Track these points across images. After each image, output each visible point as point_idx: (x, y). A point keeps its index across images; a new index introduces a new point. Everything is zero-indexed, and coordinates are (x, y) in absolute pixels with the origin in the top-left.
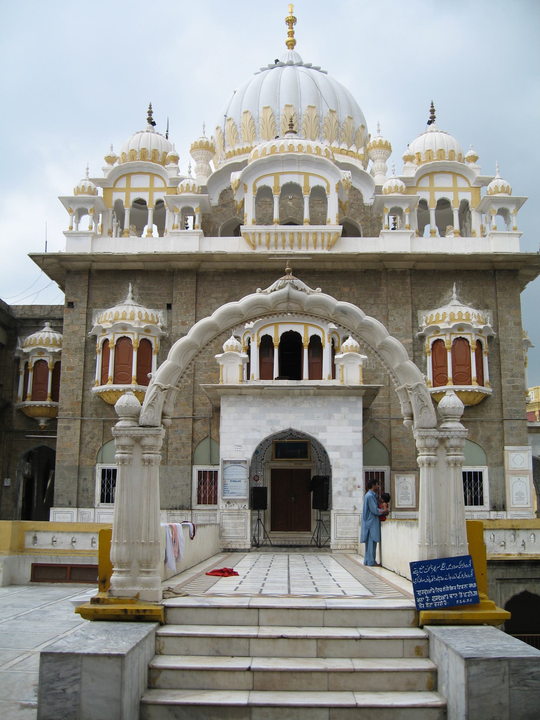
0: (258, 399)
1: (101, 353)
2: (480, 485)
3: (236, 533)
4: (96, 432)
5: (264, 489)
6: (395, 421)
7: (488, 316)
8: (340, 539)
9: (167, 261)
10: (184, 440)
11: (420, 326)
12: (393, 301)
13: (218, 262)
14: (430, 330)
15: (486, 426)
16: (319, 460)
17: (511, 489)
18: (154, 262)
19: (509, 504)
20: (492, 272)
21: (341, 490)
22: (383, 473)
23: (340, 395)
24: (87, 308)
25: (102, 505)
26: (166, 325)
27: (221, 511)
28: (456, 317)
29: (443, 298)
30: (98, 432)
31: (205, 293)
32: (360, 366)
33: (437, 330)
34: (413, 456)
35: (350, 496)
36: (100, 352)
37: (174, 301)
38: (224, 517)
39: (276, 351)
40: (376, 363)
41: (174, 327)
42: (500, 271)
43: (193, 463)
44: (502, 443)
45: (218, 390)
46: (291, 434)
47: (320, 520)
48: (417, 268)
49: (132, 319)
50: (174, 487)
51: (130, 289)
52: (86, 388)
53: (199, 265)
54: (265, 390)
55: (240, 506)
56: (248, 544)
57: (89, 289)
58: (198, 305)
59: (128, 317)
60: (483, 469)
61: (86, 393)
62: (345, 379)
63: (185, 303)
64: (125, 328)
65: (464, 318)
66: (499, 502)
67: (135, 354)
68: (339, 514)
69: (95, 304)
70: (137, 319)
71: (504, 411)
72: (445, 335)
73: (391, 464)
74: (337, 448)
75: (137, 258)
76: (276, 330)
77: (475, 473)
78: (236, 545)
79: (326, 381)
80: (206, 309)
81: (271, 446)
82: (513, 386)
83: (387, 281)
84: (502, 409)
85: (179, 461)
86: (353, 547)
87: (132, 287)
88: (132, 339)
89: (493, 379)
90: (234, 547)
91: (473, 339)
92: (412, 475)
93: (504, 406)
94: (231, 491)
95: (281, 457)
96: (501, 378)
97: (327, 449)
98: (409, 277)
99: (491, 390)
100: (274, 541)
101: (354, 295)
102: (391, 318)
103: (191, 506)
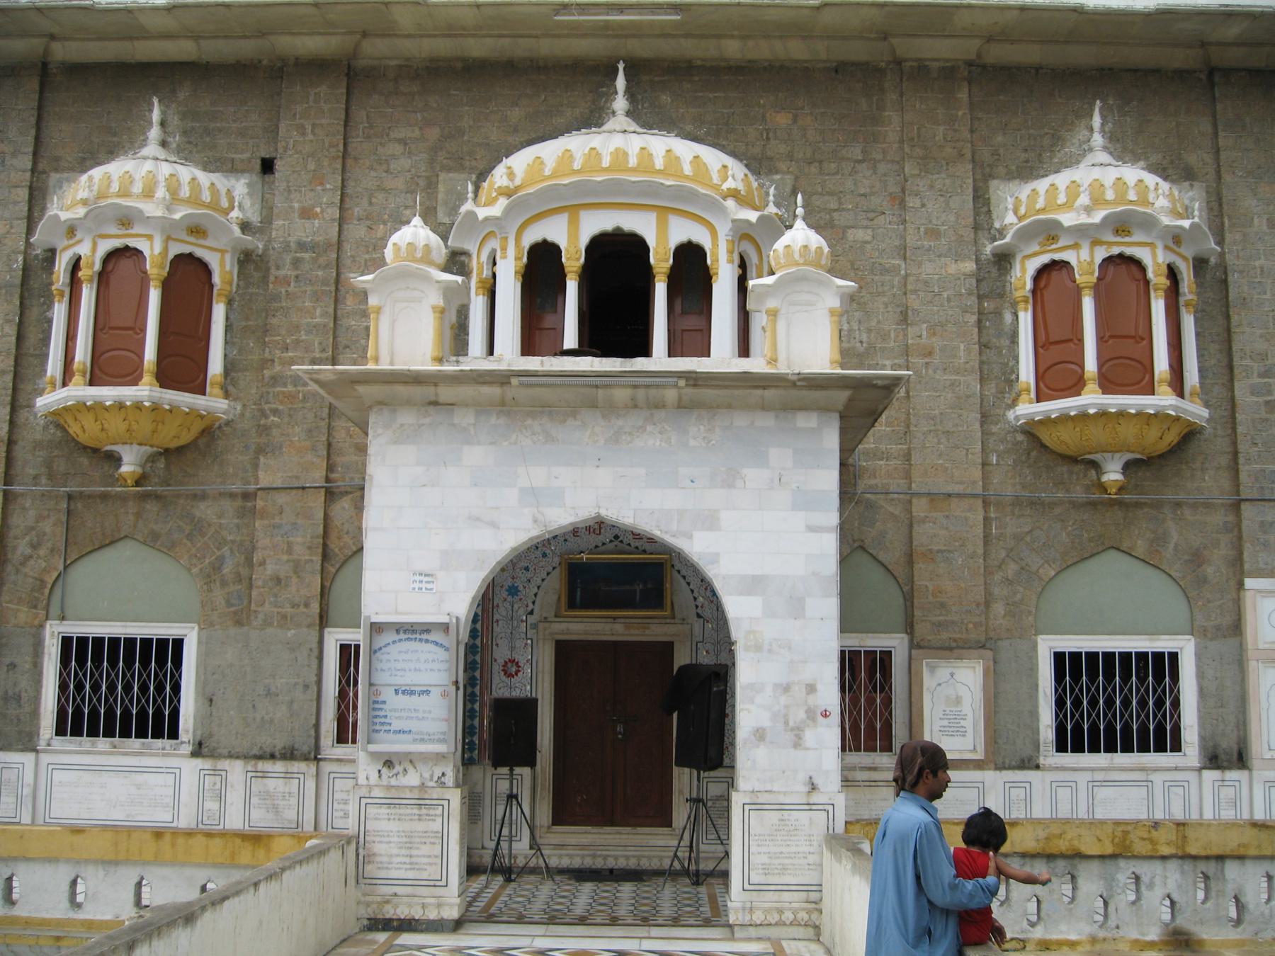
0: (493, 420)
1: (66, 298)
2: (1171, 691)
3: (413, 866)
4: (48, 530)
5: (529, 706)
6: (924, 501)
7: (1192, 200)
8: (760, 888)
9: (262, 35)
10: (300, 552)
11: (997, 225)
12: (919, 151)
13: (409, 36)
14: (1026, 234)
15: (1189, 517)
16: (699, 616)
17: (1264, 704)
18: (226, 37)
19: (1259, 748)
20: (1203, 77)
21: (766, 723)
22: (886, 655)
23: (764, 407)
24: (33, 170)
25: (59, 742)
26: (255, 218)
27: (364, 792)
28: (1110, 195)
29: (1063, 147)
30: (52, 528)
31: (371, 127)
32: (832, 312)
33: (1049, 232)
34: (978, 605)
35: (797, 745)
36: (62, 295)
37: (281, 151)
38: (372, 811)
39: (572, 287)
40: (869, 331)
41: (278, 223)
42: (1228, 72)
43: (324, 620)
44: (1238, 570)
45: (361, 389)
46: (616, 537)
47: (697, 801)
48: (989, 60)
49: (148, 194)
50: (268, 694)
51: (156, 115)
52: (22, 400)
53: (357, 45)
54: (513, 389)
55: (427, 775)
56: (451, 905)
57: (40, 119)
58: (349, 162)
59: (137, 188)
60: (1181, 644)
61: (23, 415)
62: (782, 356)
63: (312, 155)
64: (126, 220)
65: (1132, 196)
66: (1228, 743)
67: (154, 297)
68: (757, 806)
69: (57, 159)
70: (161, 192)
71: (1243, 476)
72: (1076, 246)
73: (912, 626)
74: (754, 585)
75: (169, 23)
76: (574, 225)
77: (1158, 656)
78: (410, 906)
79: (722, 356)
80: (373, 174)
81: (556, 573)
82: (1267, 403)
83: (901, 96)
84: (1234, 469)
85: (284, 617)
86: (803, 916)
87: (163, 113)
88: (147, 253)
89: (1208, 381)
90: (403, 912)
91: (1160, 259)
92: (973, 663)
93: (1241, 460)
94: (396, 725)
95: (585, 606)
96: (1231, 380)
97: (718, 585)
98: (965, 84)
99: (1205, 413)
100: (560, 856)
101: (804, 136)
102: (912, 202)
103: (317, 748)
